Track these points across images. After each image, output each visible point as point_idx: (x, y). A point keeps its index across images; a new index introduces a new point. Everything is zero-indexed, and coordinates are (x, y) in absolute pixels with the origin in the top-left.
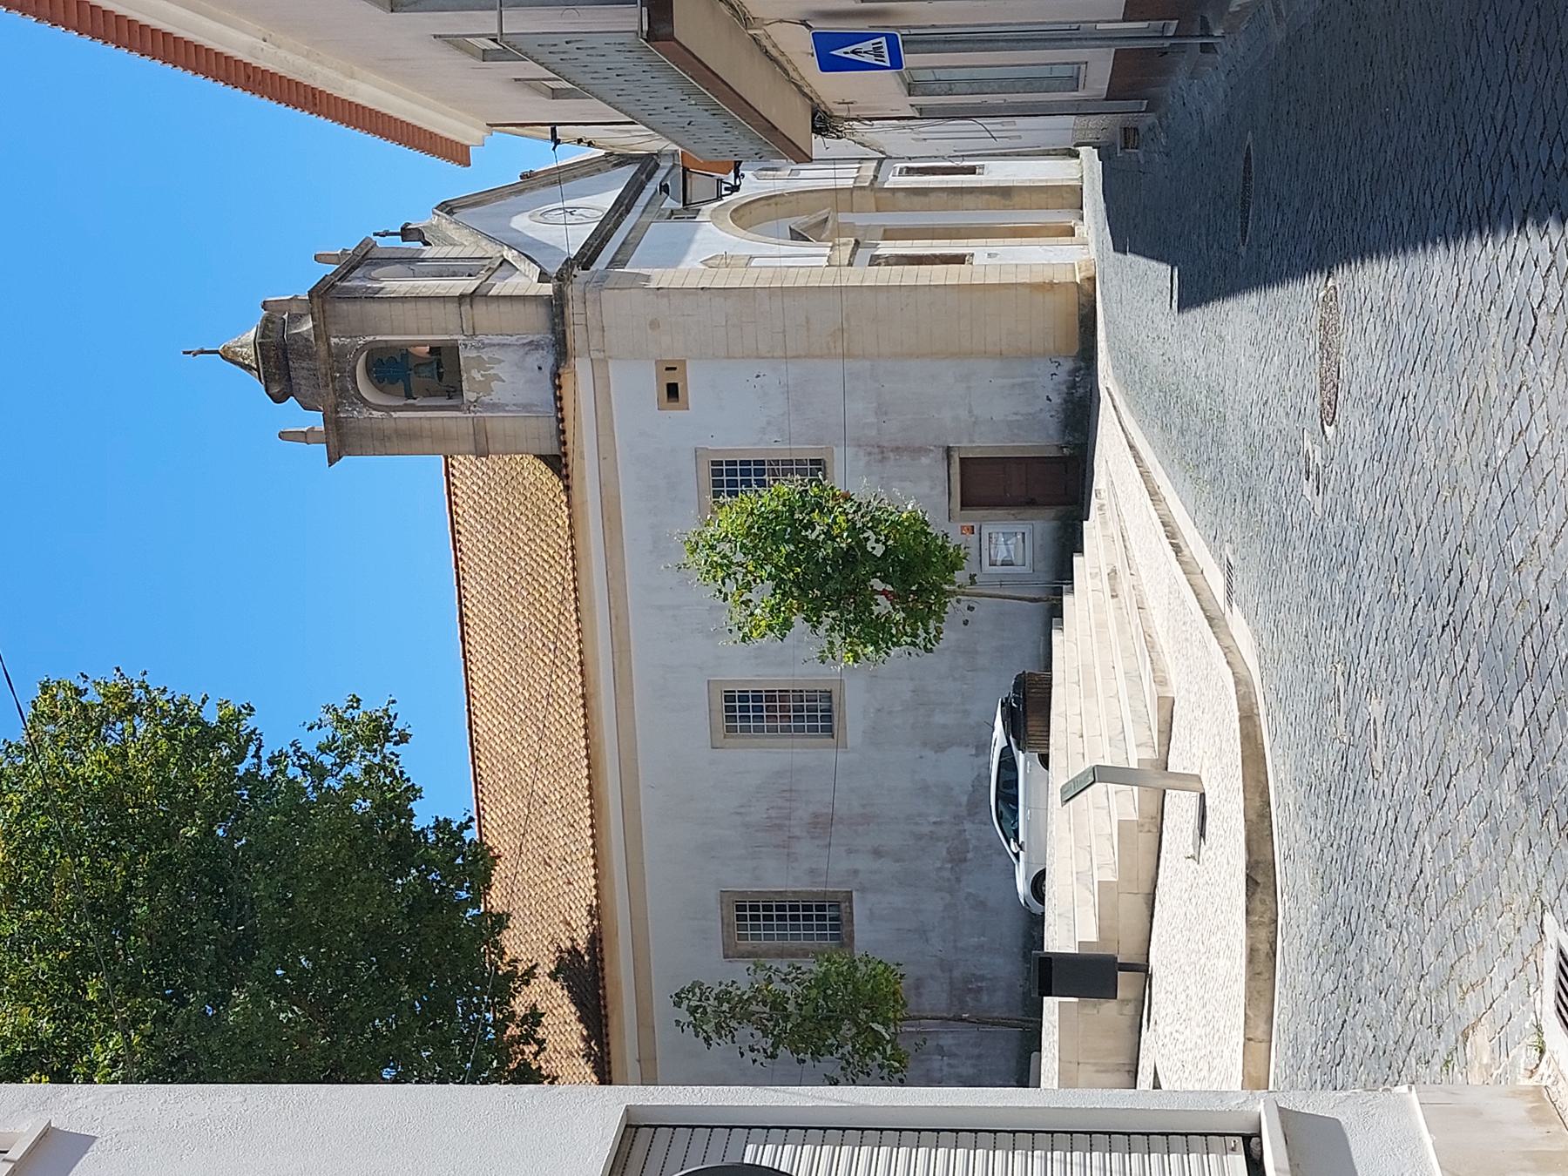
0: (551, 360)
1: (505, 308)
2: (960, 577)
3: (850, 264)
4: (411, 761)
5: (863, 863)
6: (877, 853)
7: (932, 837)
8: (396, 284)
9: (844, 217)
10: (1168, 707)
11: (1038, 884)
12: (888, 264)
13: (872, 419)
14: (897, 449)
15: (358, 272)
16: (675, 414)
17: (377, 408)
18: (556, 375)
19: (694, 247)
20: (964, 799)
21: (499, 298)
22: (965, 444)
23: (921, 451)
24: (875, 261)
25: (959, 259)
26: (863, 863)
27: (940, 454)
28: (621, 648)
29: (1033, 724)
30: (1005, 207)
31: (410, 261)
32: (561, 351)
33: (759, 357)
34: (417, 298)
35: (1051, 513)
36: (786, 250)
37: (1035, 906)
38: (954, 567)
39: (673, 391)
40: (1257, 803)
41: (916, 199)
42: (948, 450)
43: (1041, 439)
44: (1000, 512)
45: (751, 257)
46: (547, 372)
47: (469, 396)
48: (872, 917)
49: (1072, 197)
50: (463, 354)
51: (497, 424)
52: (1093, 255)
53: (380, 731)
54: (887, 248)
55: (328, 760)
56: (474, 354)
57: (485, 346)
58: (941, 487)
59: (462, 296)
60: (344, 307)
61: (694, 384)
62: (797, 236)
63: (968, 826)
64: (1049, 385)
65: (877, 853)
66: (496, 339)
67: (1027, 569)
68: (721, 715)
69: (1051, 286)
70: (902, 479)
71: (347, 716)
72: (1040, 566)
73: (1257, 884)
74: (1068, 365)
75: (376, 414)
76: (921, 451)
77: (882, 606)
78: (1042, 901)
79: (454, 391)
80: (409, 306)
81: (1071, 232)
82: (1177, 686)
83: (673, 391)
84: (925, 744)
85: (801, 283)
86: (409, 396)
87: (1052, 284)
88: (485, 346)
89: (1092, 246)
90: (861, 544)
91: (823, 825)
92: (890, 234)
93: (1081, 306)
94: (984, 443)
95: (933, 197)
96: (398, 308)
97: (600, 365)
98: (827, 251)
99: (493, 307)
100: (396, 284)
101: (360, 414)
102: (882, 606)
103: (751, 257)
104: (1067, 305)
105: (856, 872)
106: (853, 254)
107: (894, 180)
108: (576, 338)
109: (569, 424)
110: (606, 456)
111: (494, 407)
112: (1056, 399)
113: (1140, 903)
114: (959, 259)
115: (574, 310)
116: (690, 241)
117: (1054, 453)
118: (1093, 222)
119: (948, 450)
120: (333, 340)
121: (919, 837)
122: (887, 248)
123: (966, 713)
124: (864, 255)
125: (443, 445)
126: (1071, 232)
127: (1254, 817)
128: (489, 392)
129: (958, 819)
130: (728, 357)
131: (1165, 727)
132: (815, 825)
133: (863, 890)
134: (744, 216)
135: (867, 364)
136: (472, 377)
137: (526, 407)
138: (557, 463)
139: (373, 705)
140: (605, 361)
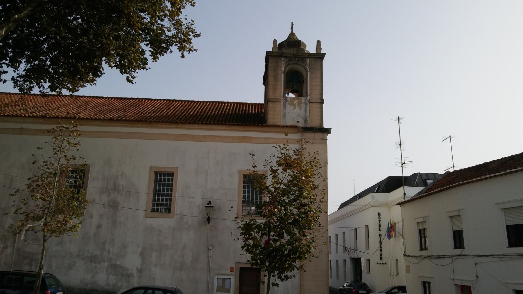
6: (99, 227)
20: (118, 263)
26: (95, 221)
63: (106, 264)
83: (236, 229)
84: (144, 248)
88: (306, 105)
91: (114, 206)
105: (91, 217)
111: (285, 106)
121: (104, 244)
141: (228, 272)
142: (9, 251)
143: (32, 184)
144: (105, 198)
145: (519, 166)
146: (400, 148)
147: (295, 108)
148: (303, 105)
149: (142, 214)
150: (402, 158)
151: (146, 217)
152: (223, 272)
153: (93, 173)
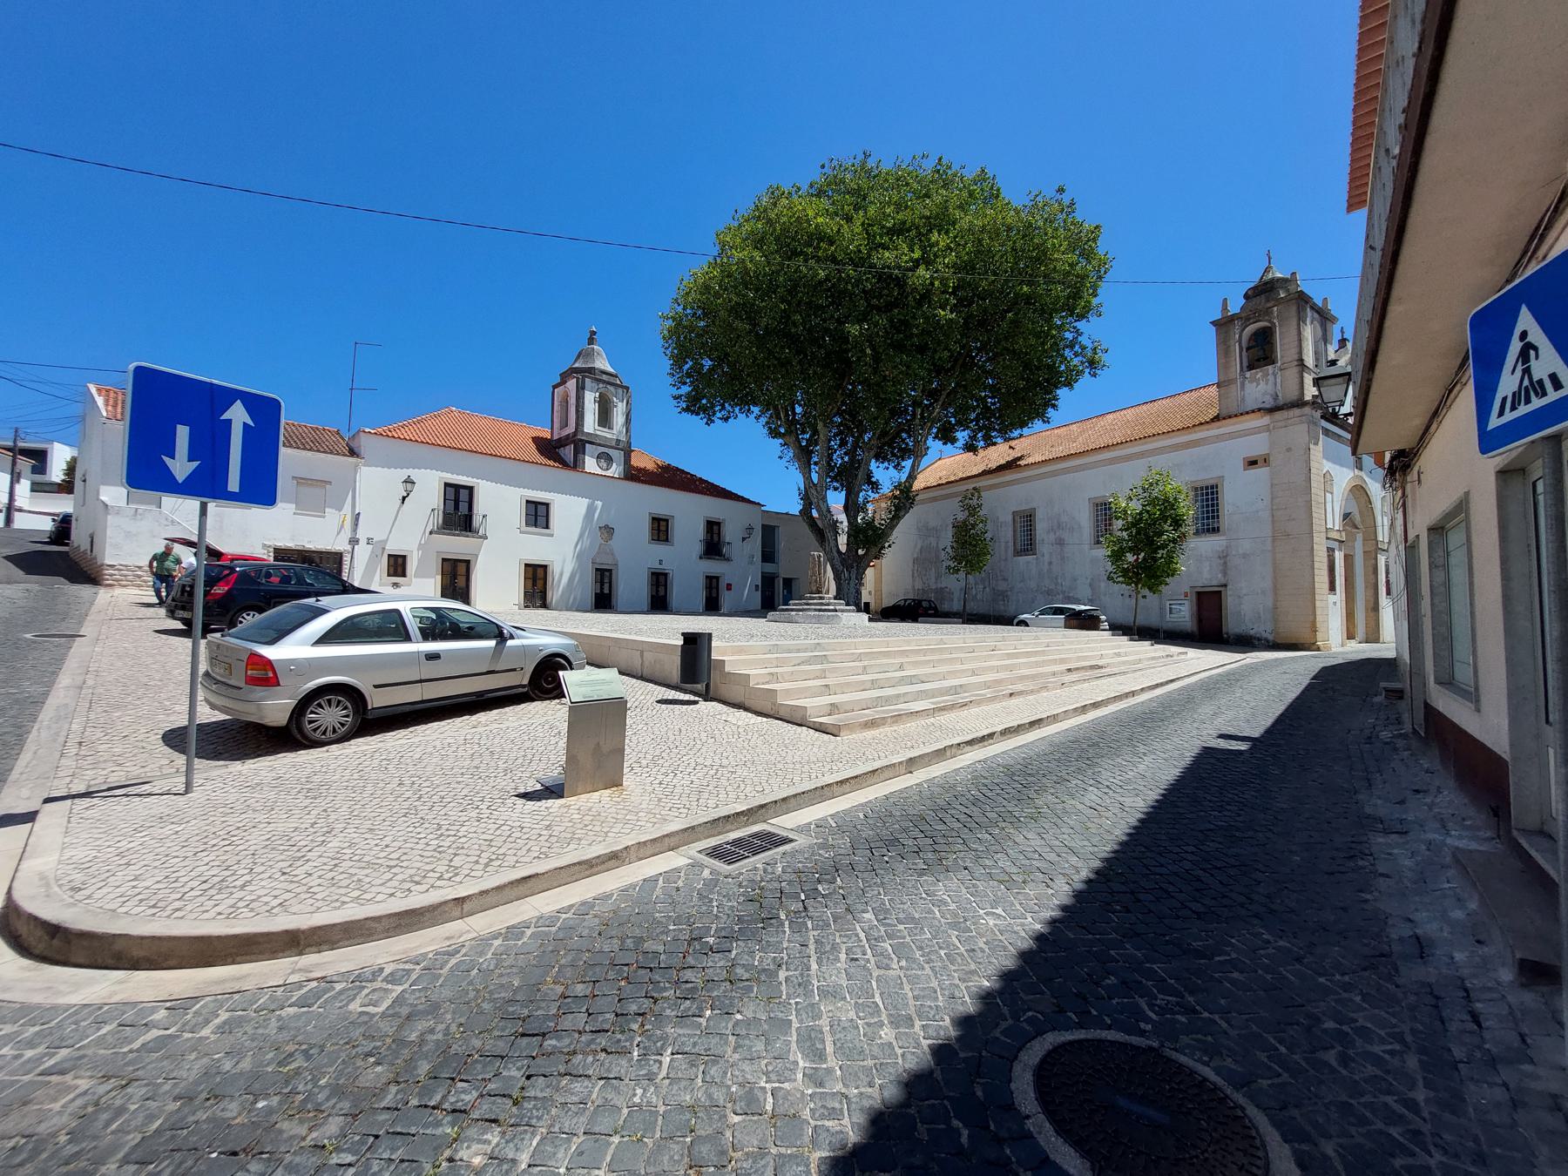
0: (1268, 406)
1: (1297, 381)
2: (1146, 592)
3: (1328, 538)
4: (1085, 381)
5: (1047, 558)
6: (1050, 563)
7: (1056, 584)
8: (1309, 332)
9: (1360, 537)
10: (835, 732)
11: (1024, 623)
12: (1329, 556)
13: (1241, 551)
14: (1225, 563)
15: (1316, 315)
16: (1241, 465)
17: (1240, 337)
18: (1259, 410)
19: (1337, 467)
20: (1071, 595)
21: (1302, 378)
22: (1229, 593)
23: (1225, 573)
24: (1330, 550)
25: (1332, 588)
26: (1047, 558)
27: (1223, 582)
28: (1129, 458)
29: (1075, 622)
30: (1367, 609)
31: (1325, 338)
32: (1271, 411)
33: (1272, 499)
34: (1300, 340)
35: (1195, 629)
36: (1337, 509)
37: (1015, 621)
38: (1150, 589)
39: (1253, 463)
40: (137, 953)
41: (1371, 569)
42: (1225, 586)
43: (1231, 626)
44: (1195, 608)
45: (1332, 493)
46: (1262, 406)
47: (1248, 374)
48: (1028, 562)
49: (1373, 636)
50: (1270, 367)
51: (1234, 390)
52: (1334, 650)
53: (1092, 363)
54: (1339, 557)
55: (1077, 348)
56: (1270, 372)
57: (1275, 376)
58: (1206, 583)
59: (1302, 360)
60: (1294, 308)
61: (1260, 472)
62: (1346, 516)
63: (1061, 596)
64: (1262, 629)
65: (1050, 563)
66: (1279, 380)
67: (1168, 619)
68: (1100, 501)
69: (1314, 630)
70: (1210, 566)
71: (1098, 351)
72: (1170, 625)
73: (53, 937)
74: (1270, 638)
75: (1237, 336)
76: (1225, 573)
77: (1130, 558)
78: (1017, 625)
79: (1251, 367)
80: (1296, 338)
81: (1350, 636)
82: (846, 738)
83: (1253, 463)
84: (1092, 579)
85: (1314, 515)
86: (1248, 349)
87: (1316, 631)
88: (1275, 376)
89: (1341, 649)
90: (1159, 548)
91: (1060, 542)
92: (1348, 559)
93: (1302, 644)
94: (1230, 601)
95: (1373, 577)
96: (1295, 332)
97: (1267, 428)
98: (1337, 528)
99: (1297, 375)
100: (1309, 332)
101: (1237, 329)
102: (1130, 558)
103: (1332, 493)
104: (1304, 635)
105: (1043, 555)
106: (1336, 540)
107: (1382, 560)
108: (1279, 415)
109: (1235, 419)
110: (1220, 438)
111: (1243, 385)
112: (1252, 632)
113: (738, 699)
114: (1332, 588)
115: (1297, 411)
116: (1342, 465)
117: (1224, 630)
118: (1357, 650)
119: (1225, 586)
120: (1275, 309)
121: (1056, 579)
122: (1339, 557)
123: (1105, 595)
124: (1335, 545)
125: (1223, 365)
126: (1350, 636)
127: (118, 946)
128: (1250, 382)
129: (1064, 592)
130: (1272, 485)
131: (823, 728)
132: (1060, 539)
133: (1037, 559)
134: (1359, 491)
135: (1270, 548)
136: (1259, 373)
137: (1243, 399)
138: (1216, 419)
139: (1105, 358)
140: (1269, 430)
141: (1182, 597)
142: (987, 589)
143: (242, 684)
144: (1052, 537)
145: (832, 543)
146: (14, 885)
147: (1258, 384)
148: (1271, 378)
149: (1087, 547)
150: (421, 681)
151: (1091, 549)
152: (1178, 597)
153: (1039, 515)
